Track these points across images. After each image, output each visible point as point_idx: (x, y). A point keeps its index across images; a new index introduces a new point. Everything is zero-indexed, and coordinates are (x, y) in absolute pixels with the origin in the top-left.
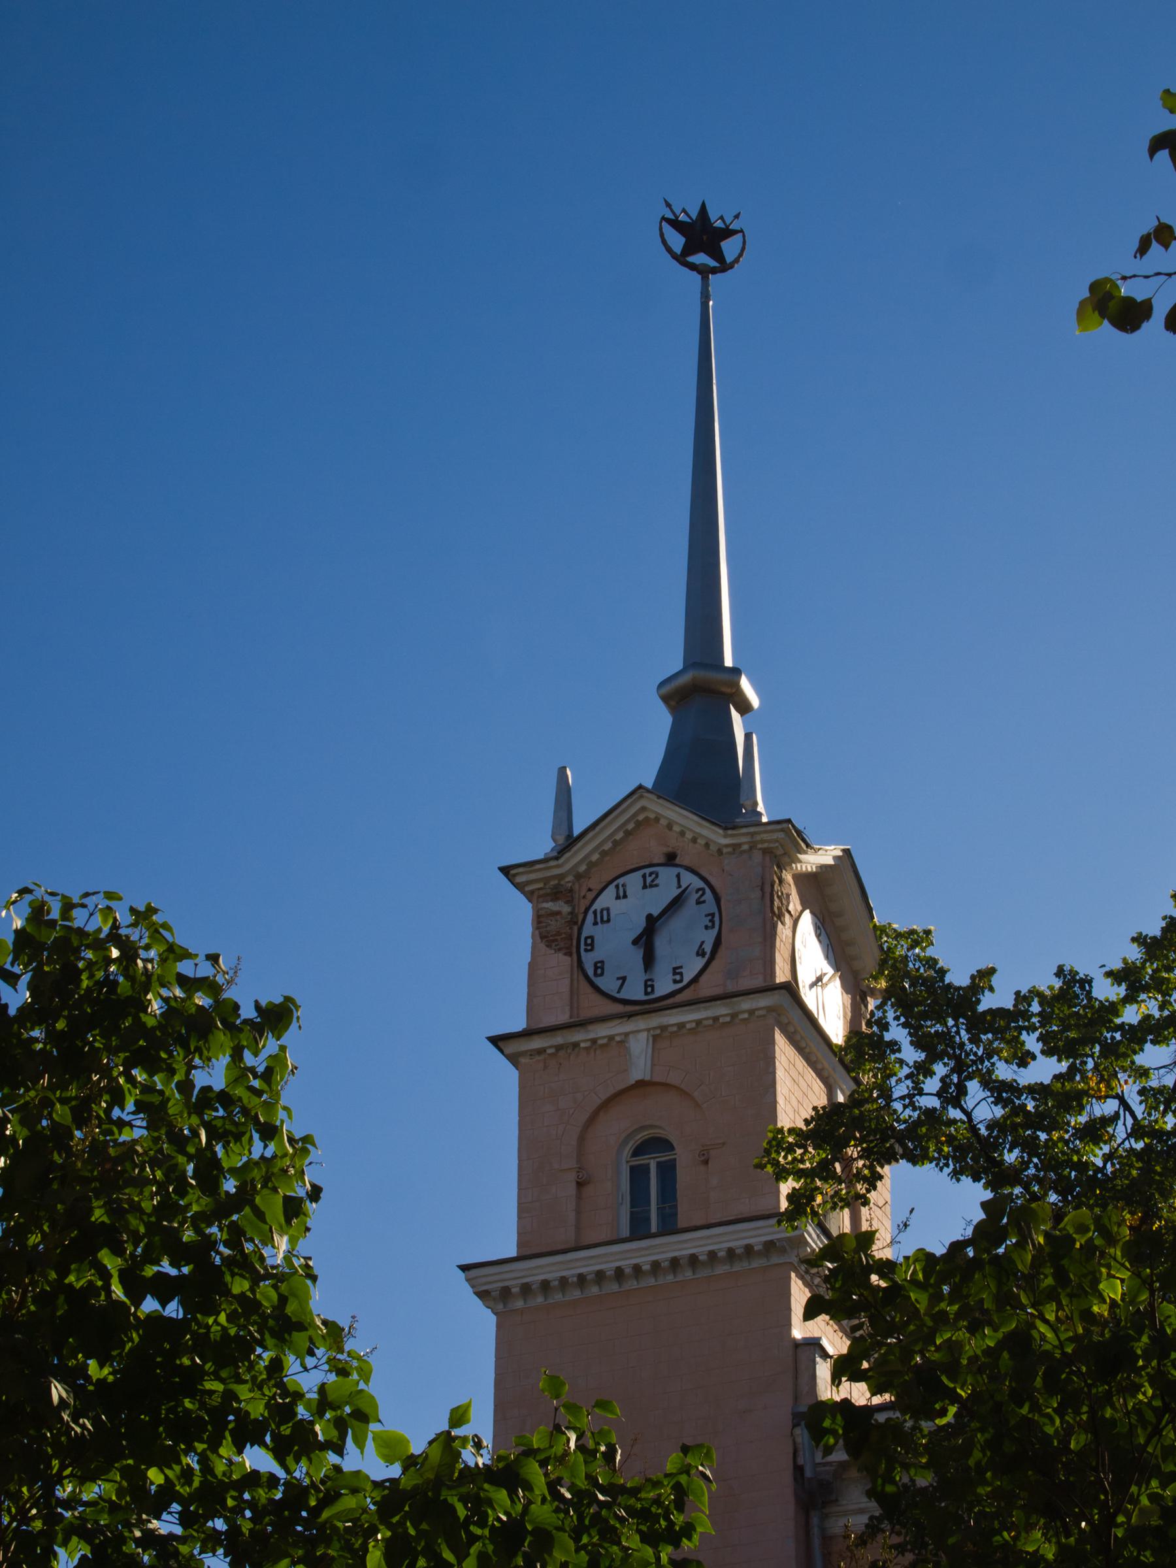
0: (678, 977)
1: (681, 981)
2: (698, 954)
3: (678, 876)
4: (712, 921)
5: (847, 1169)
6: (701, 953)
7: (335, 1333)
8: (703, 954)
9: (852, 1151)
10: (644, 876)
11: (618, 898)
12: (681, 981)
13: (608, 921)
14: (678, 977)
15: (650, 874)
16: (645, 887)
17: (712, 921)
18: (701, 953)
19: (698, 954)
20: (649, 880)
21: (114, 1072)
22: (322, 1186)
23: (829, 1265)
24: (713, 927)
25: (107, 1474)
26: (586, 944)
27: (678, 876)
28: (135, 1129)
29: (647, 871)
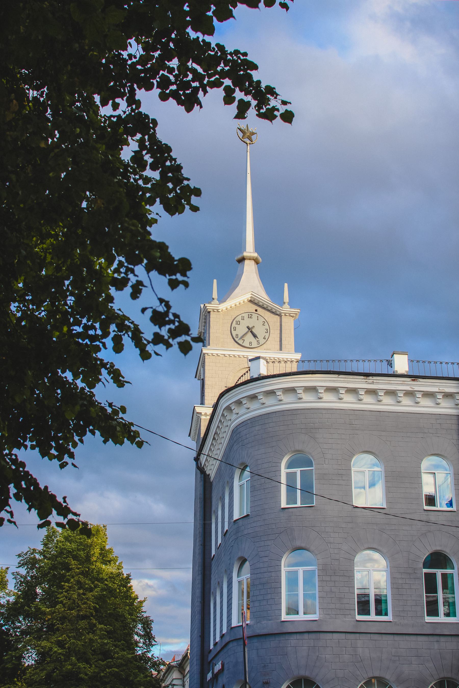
0: (258, 343)
1: (259, 344)
2: (264, 338)
3: (258, 317)
4: (267, 331)
5: (230, 598)
6: (264, 338)
7: (108, 362)
8: (265, 339)
9: (89, 527)
10: (249, 315)
11: (242, 319)
12: (259, 344)
13: (239, 324)
14: (258, 343)
15: (250, 315)
16: (249, 318)
17: (267, 331)
18: (264, 338)
19: (264, 338)
20: (250, 316)
21: (187, 10)
22: (189, 113)
23: (41, 283)
24: (267, 333)
25: (63, 459)
26: (234, 329)
27: (258, 317)
28: (161, 306)
29: (250, 314)
